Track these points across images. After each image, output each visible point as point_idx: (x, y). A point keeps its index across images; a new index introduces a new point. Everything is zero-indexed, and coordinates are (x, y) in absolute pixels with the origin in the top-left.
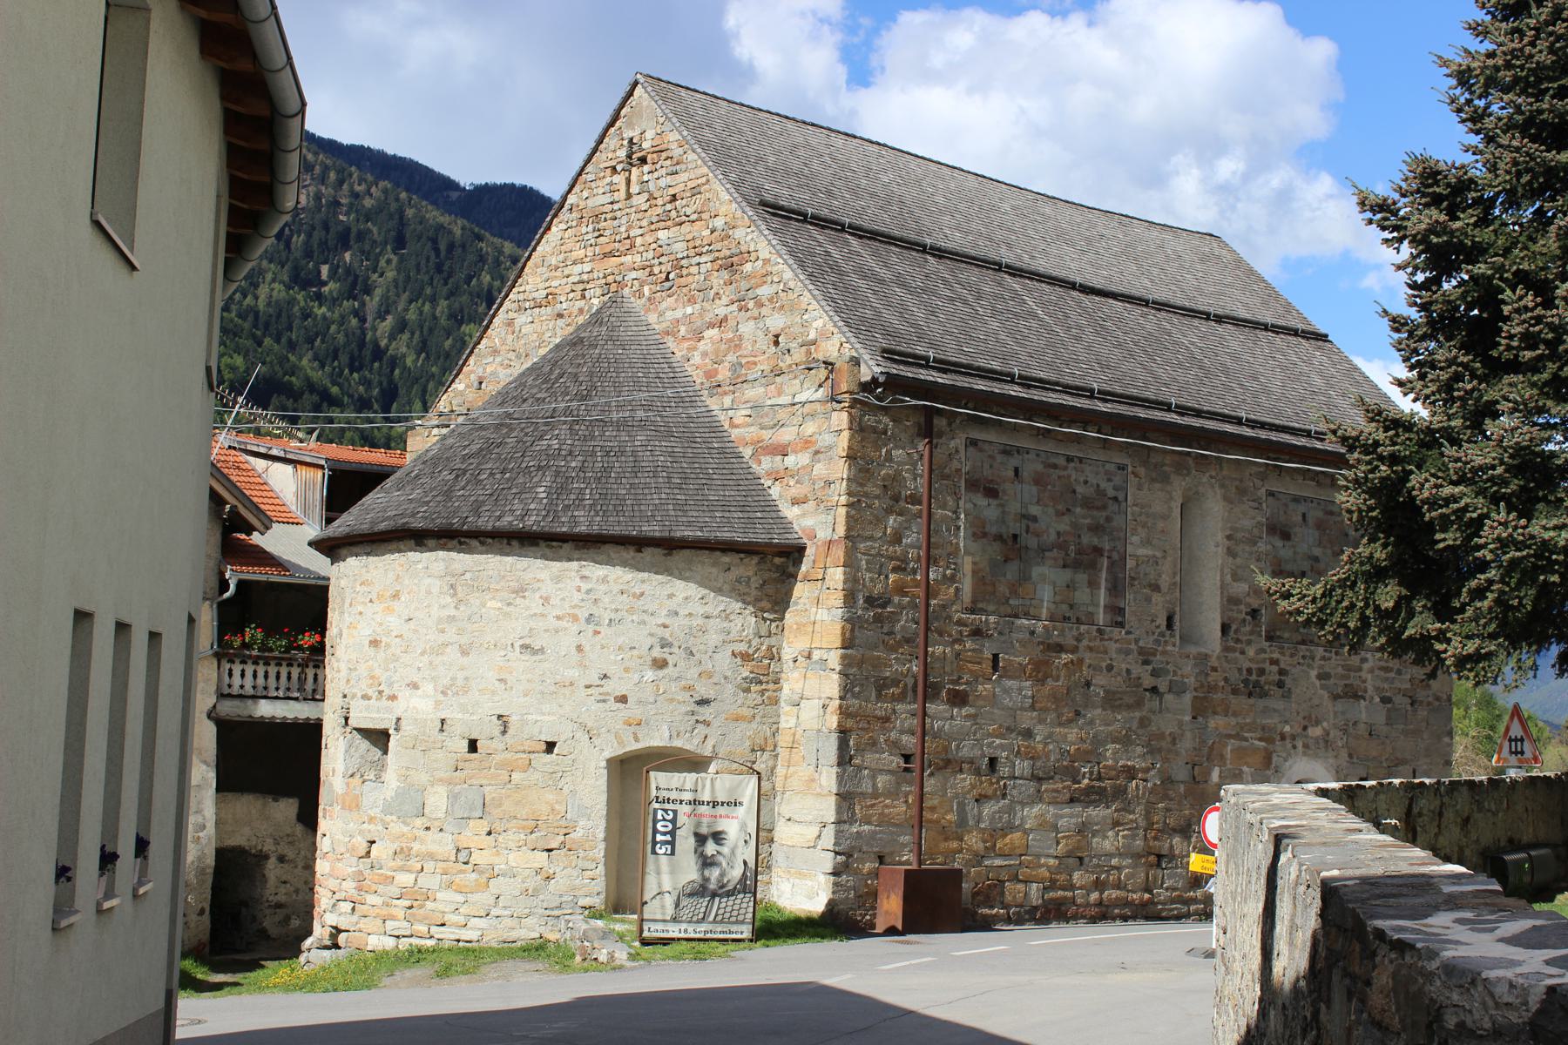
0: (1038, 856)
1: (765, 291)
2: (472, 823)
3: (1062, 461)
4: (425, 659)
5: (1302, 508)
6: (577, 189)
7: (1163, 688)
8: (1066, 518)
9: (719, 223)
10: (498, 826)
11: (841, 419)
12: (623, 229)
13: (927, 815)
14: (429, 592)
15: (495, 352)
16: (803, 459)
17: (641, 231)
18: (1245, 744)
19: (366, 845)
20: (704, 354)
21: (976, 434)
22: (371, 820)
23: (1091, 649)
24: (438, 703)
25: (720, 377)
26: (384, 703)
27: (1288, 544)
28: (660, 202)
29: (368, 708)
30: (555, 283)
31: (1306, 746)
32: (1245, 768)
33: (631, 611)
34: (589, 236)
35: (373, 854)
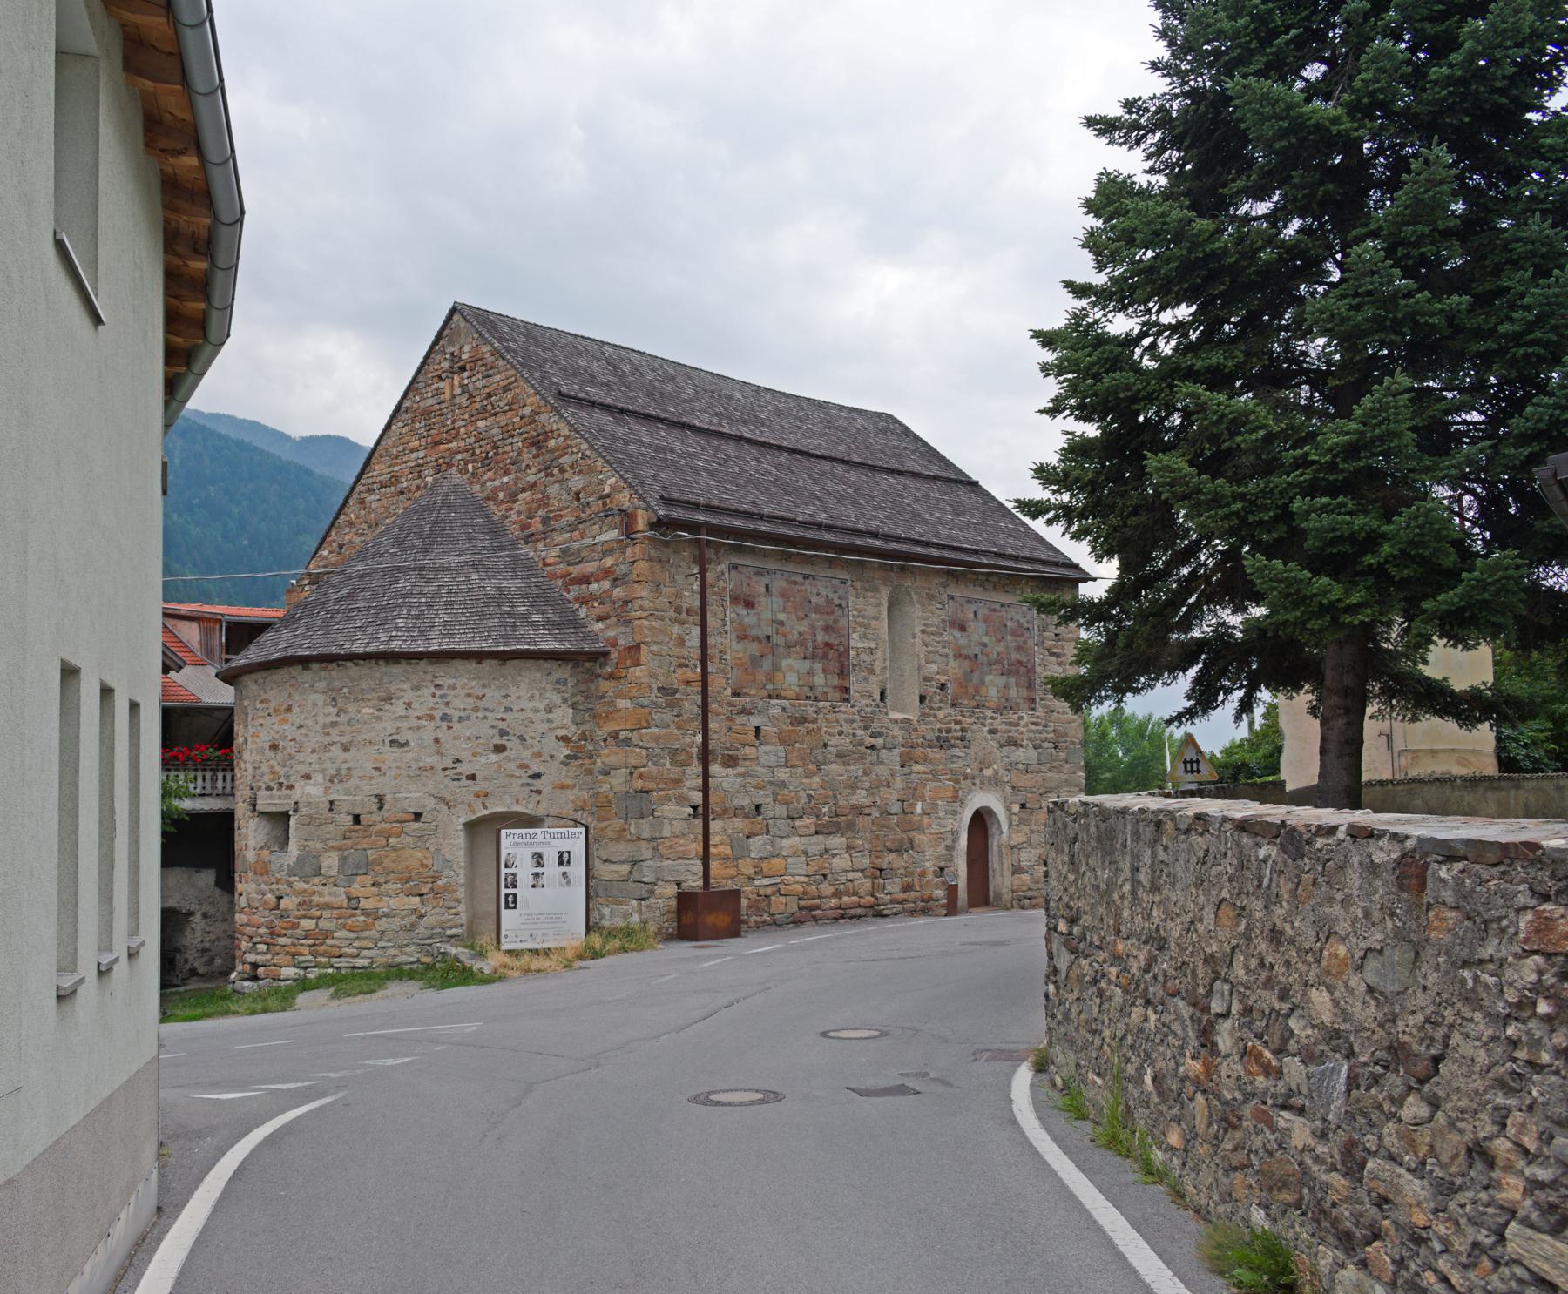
1: (566, 460)
3: (800, 579)
4: (315, 756)
5: (974, 607)
6: (411, 395)
8: (805, 622)
9: (527, 411)
10: (381, 879)
13: (712, 850)
14: (315, 705)
15: (351, 524)
16: (606, 584)
20: (519, 513)
21: (736, 560)
24: (327, 789)
26: (285, 792)
29: (271, 797)
31: (982, 783)
33: (476, 709)
35: (282, 906)
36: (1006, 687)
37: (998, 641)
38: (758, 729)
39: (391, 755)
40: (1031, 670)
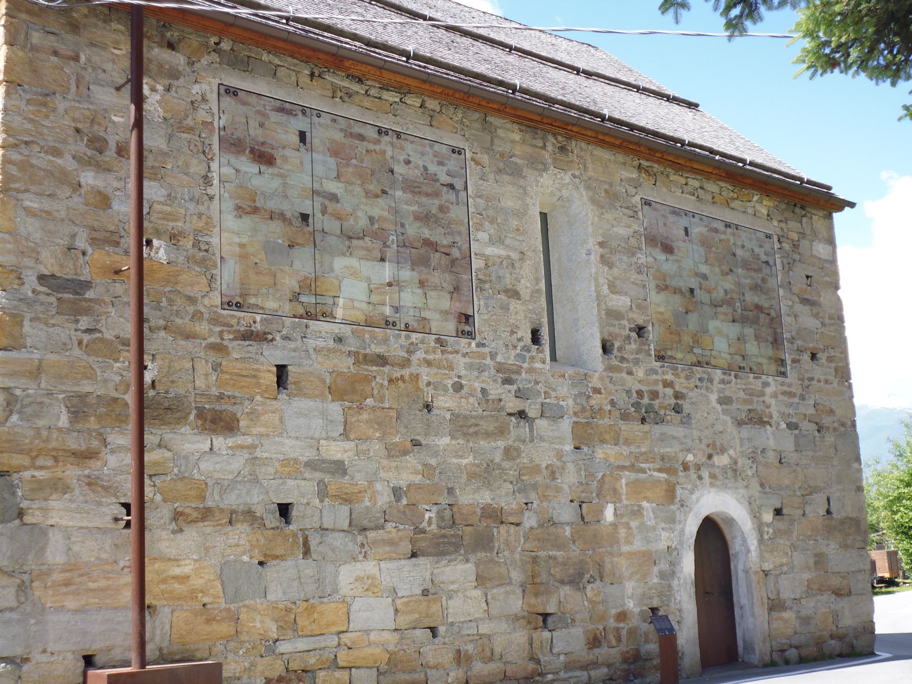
21: (234, 81)
27: (671, 258)
31: (713, 476)
32: (645, 504)
38: (281, 370)
40: (775, 321)
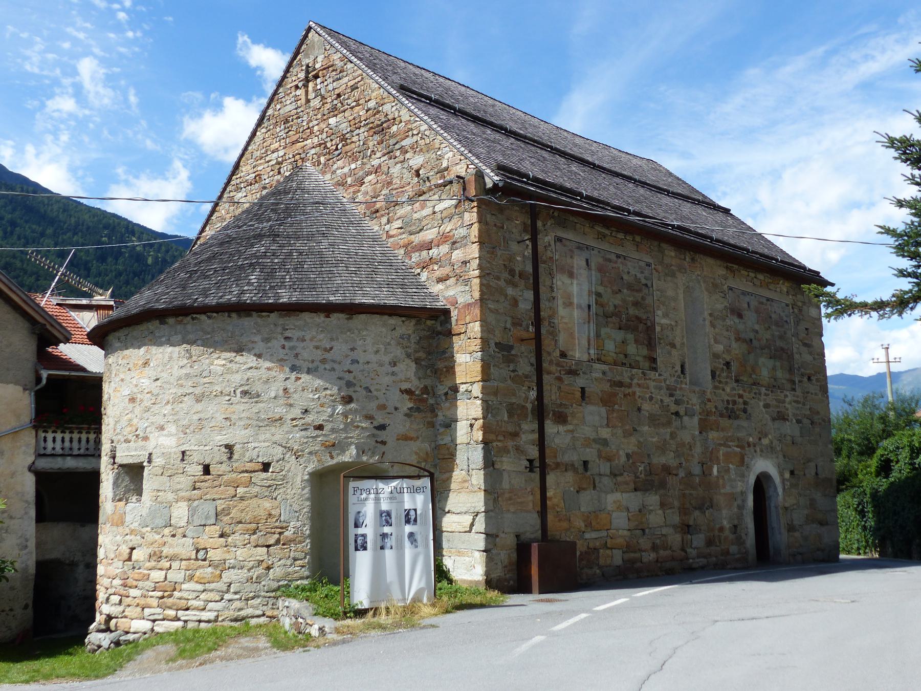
0: (617, 530)
1: (406, 142)
2: (207, 528)
3: (613, 257)
4: (169, 407)
5: (747, 299)
7: (682, 413)
10: (227, 530)
11: (471, 217)
12: (304, 124)
16: (444, 249)
17: (316, 122)
18: (729, 450)
19: (128, 551)
22: (132, 532)
23: (639, 385)
25: (378, 206)
26: (141, 443)
28: (329, 100)
29: (128, 449)
30: (260, 168)
31: (762, 451)
32: (731, 466)
33: (323, 361)
34: (282, 133)
35: (134, 557)
36: (774, 369)
37: (627, 434)
38: (583, 389)
39: (241, 408)
